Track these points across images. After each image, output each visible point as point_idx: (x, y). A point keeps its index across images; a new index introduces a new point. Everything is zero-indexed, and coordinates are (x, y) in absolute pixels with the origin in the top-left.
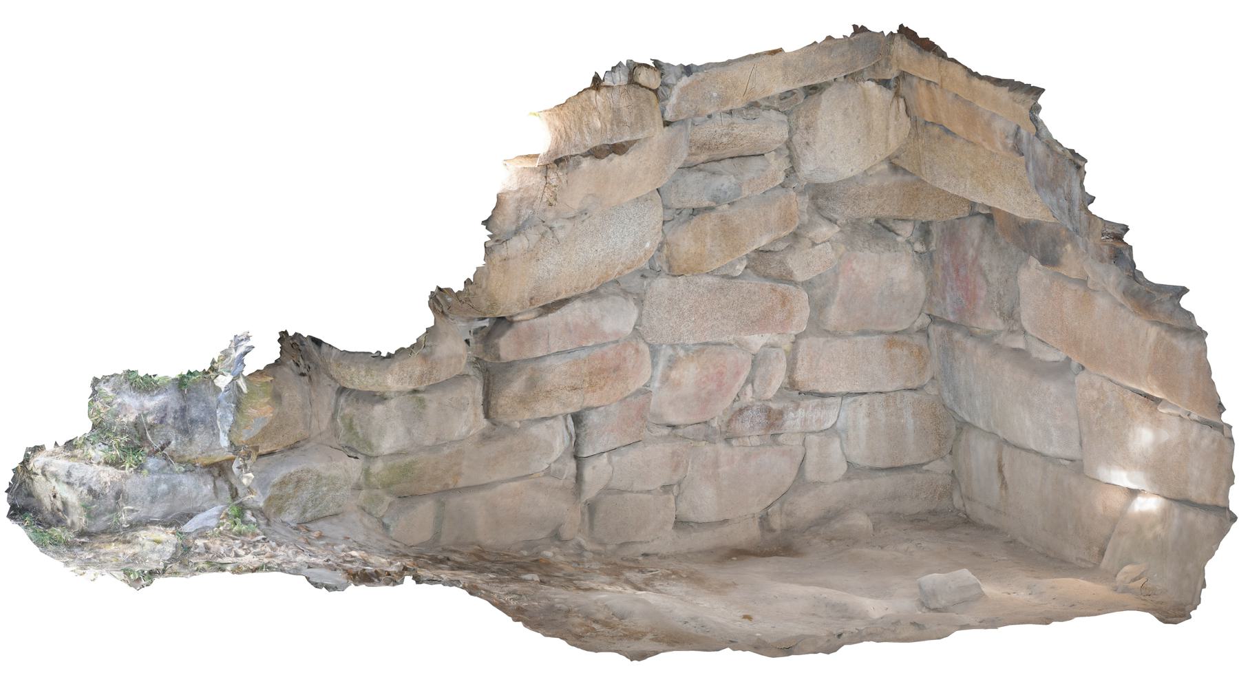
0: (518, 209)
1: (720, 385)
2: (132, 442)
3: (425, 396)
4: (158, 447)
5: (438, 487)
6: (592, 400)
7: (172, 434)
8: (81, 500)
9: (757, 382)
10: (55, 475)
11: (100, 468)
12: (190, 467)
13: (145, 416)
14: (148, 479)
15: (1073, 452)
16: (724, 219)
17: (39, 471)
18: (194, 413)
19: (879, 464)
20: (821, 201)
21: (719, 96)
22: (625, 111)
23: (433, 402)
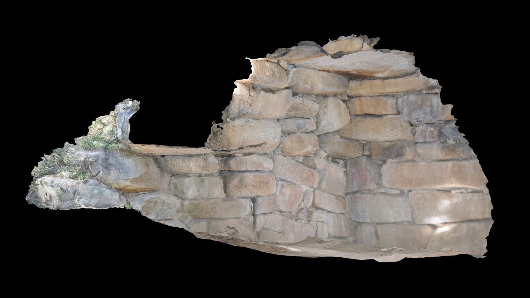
0: (239, 104)
1: (296, 199)
2: (82, 170)
3: (204, 178)
4: (95, 174)
5: (208, 216)
6: (260, 193)
7: (101, 168)
8: (57, 193)
9: (305, 201)
10: (46, 183)
11: (67, 179)
12: (109, 186)
13: (89, 158)
14: (89, 187)
15: (409, 219)
16: (299, 137)
17: (39, 183)
18: (111, 161)
19: (337, 235)
20: (322, 145)
21: (304, 80)
22: (276, 72)
23: (207, 180)
